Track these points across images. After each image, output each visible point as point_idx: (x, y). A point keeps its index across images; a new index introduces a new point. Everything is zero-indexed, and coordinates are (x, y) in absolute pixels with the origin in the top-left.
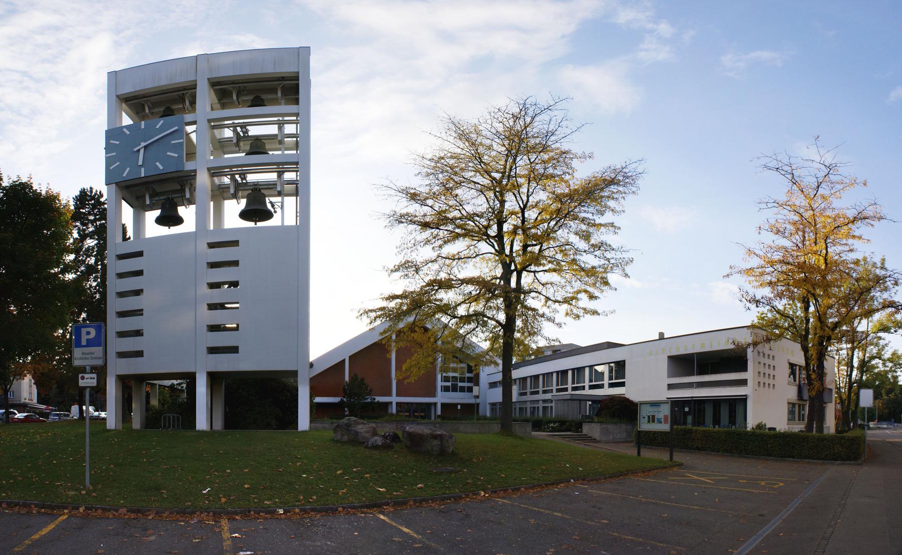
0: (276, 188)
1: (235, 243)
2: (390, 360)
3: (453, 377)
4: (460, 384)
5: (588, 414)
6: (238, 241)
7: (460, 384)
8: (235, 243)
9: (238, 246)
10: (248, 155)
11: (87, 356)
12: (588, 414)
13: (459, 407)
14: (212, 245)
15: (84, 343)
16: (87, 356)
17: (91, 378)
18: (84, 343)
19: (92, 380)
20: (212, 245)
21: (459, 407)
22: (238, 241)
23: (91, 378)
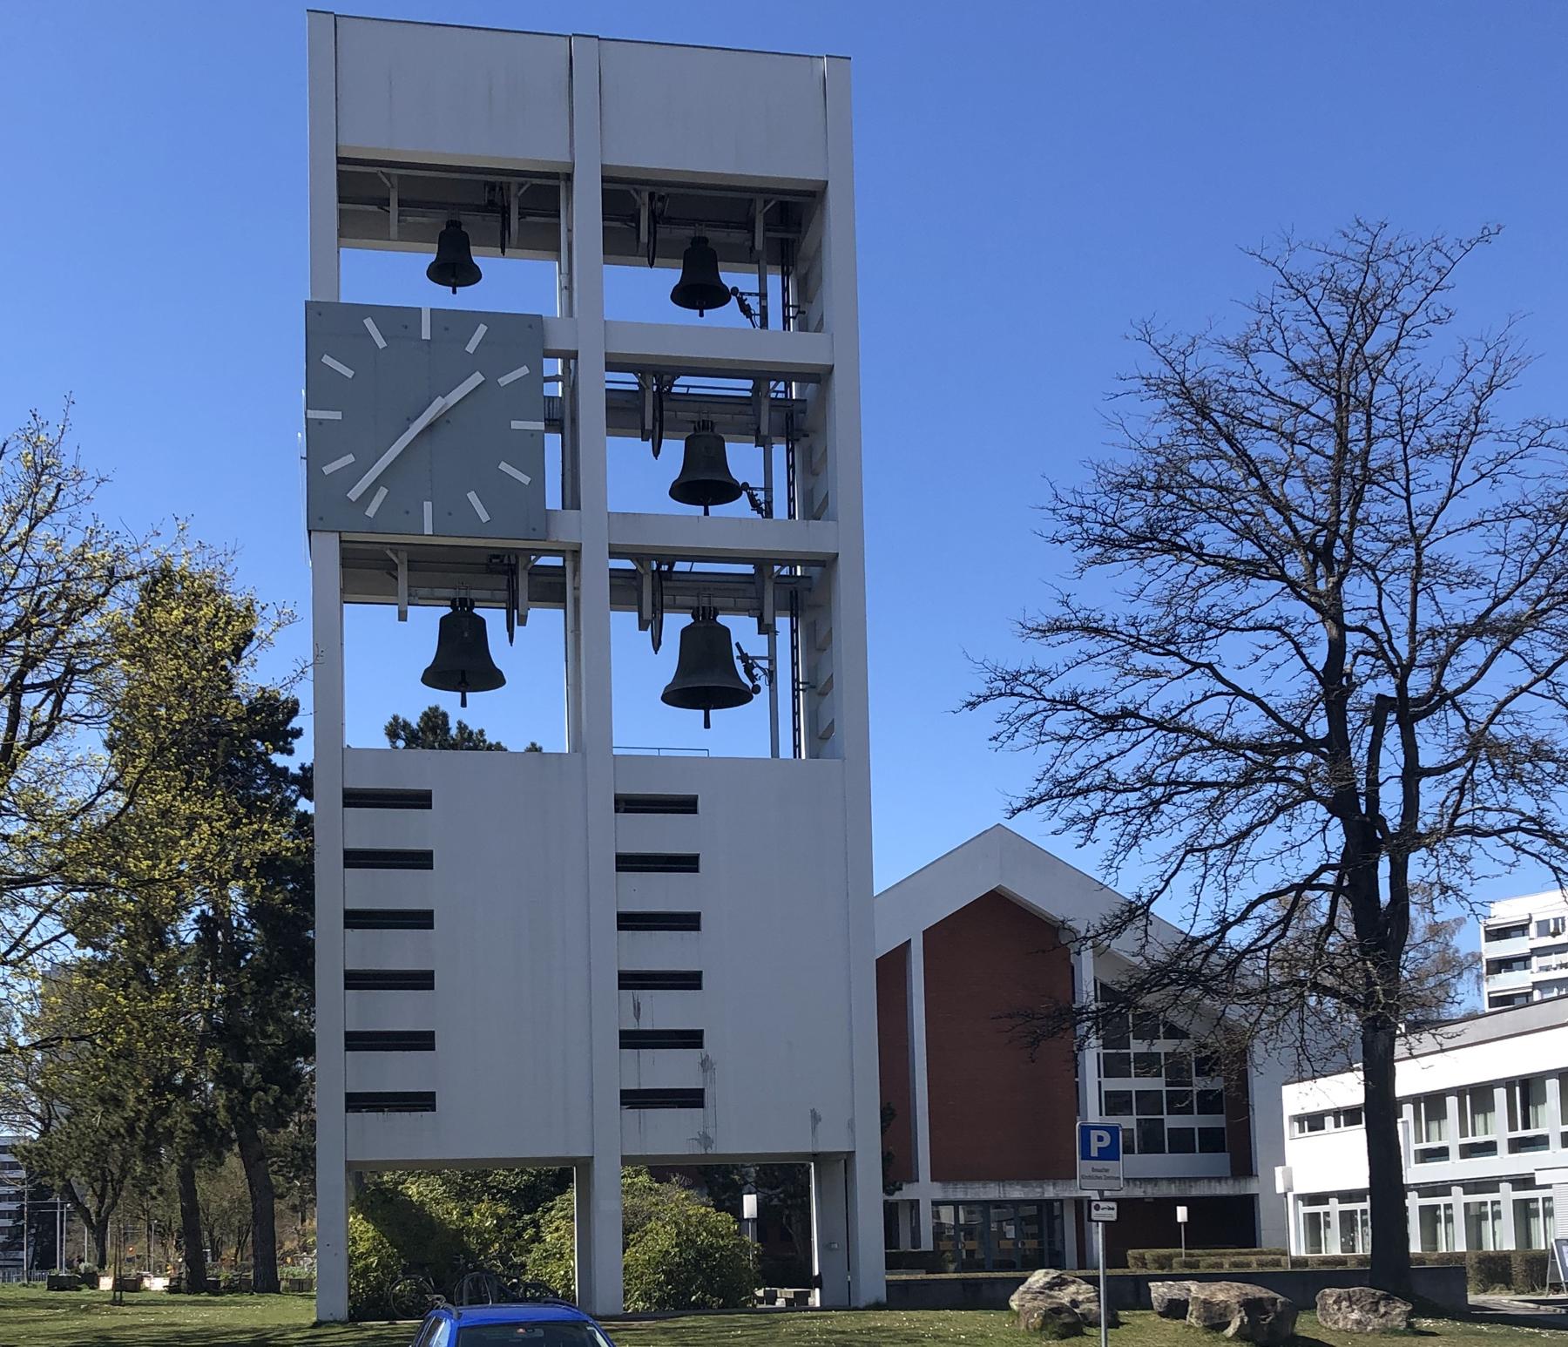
0: (704, 608)
1: (687, 805)
2: (1356, 1220)
3: (1188, 1111)
4: (1171, 1122)
5: (354, 494)
6: (431, 1035)
7: (1171, 1122)
8: (687, 805)
9: (431, 987)
10: (659, 453)
11: (1099, 1174)
12: (354, 494)
13: (1182, 1214)
14: (628, 804)
15: (1094, 1153)
16: (1099, 1174)
17: (1110, 1209)
18: (1094, 1153)
19: (1111, 1212)
20: (628, 804)
21: (1182, 1214)
22: (431, 1035)
23: (1110, 1209)
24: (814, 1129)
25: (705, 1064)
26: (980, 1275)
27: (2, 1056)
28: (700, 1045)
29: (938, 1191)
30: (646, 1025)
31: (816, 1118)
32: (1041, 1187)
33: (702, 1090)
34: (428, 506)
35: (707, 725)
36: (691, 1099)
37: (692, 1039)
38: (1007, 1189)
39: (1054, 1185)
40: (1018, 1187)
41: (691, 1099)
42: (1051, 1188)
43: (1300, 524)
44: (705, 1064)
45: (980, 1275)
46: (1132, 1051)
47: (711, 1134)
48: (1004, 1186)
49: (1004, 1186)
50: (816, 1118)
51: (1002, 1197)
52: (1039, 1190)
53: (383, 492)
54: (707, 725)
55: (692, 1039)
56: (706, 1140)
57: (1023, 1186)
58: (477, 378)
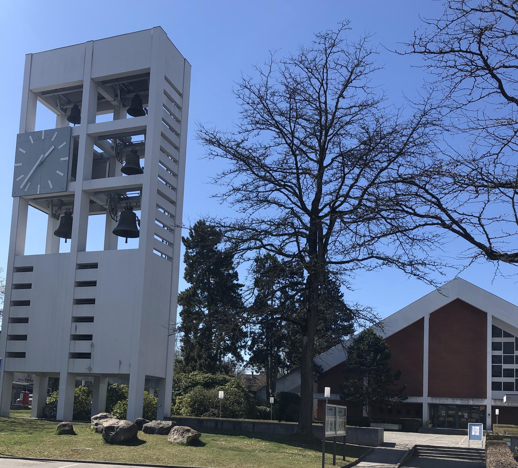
5: (21, 187)
24: (120, 366)
25: (92, 345)
26: (294, 423)
27: (514, 366)
28: (91, 340)
29: (430, 400)
30: (78, 333)
31: (120, 363)
32: (468, 400)
33: (90, 353)
34: (39, 186)
35: (126, 242)
36: (87, 356)
37: (89, 337)
38: (455, 400)
39: (473, 400)
40: (459, 400)
41: (87, 356)
42: (472, 401)
43: (409, 142)
44: (92, 345)
45: (294, 423)
46: (515, 355)
47: (91, 366)
48: (454, 400)
49: (454, 400)
50: (120, 363)
51: (453, 403)
52: (467, 402)
53: (29, 183)
54: (126, 242)
55: (89, 337)
56: (90, 368)
57: (461, 400)
58: (53, 147)
